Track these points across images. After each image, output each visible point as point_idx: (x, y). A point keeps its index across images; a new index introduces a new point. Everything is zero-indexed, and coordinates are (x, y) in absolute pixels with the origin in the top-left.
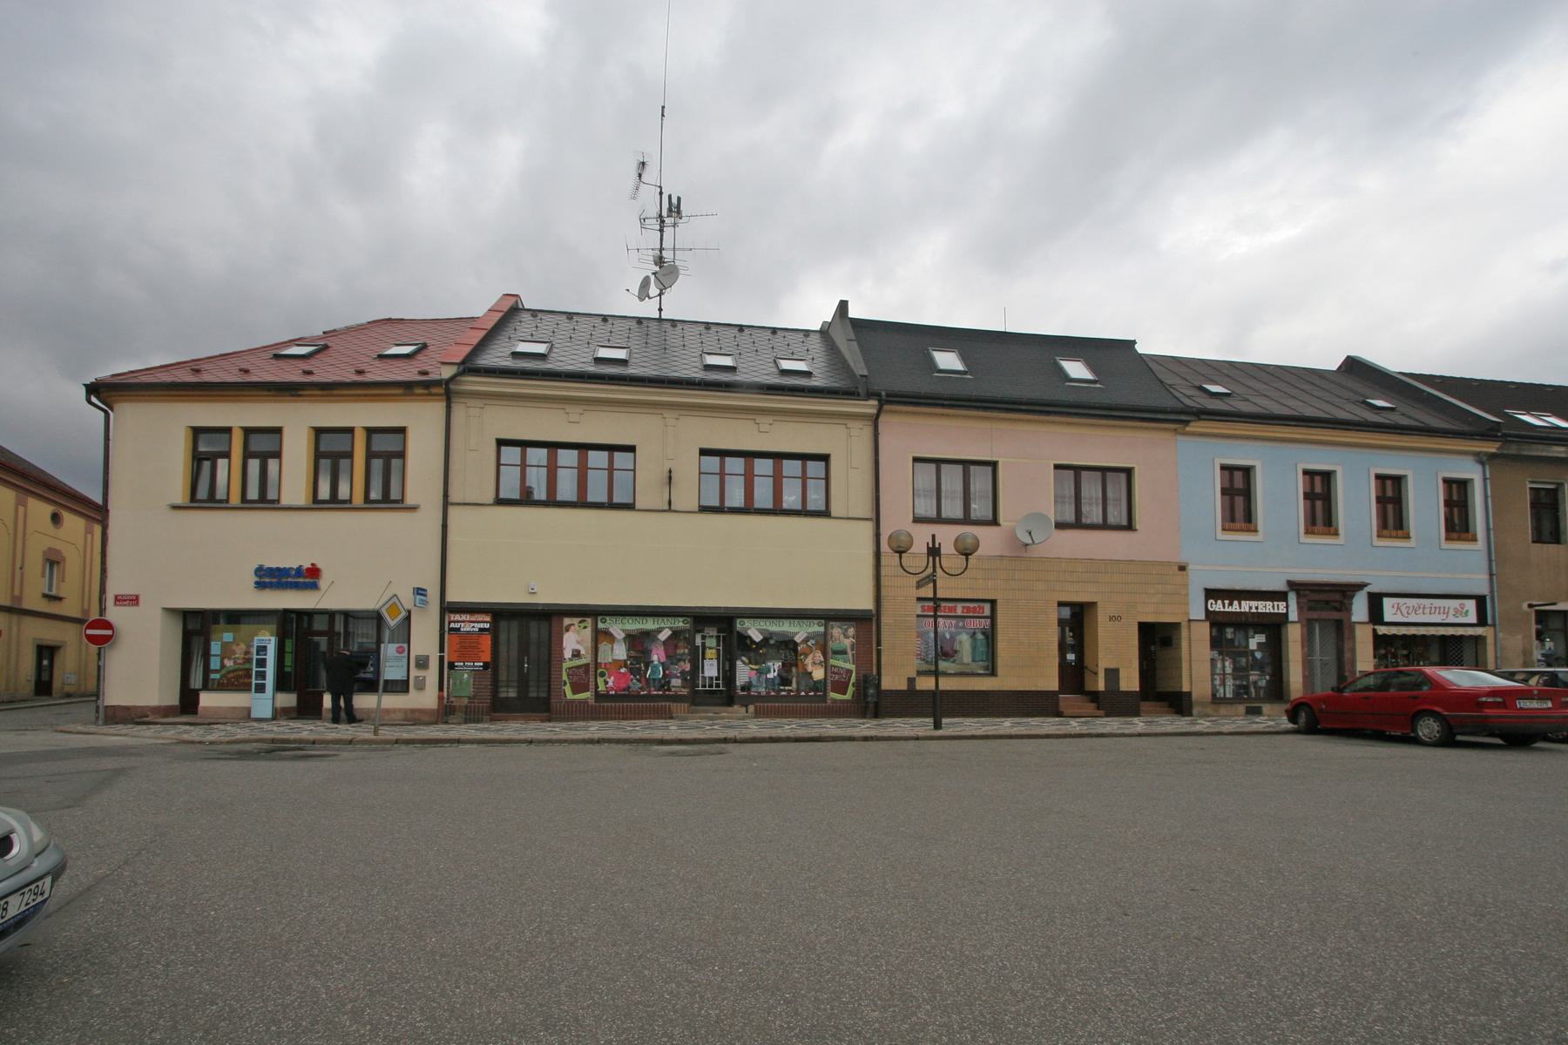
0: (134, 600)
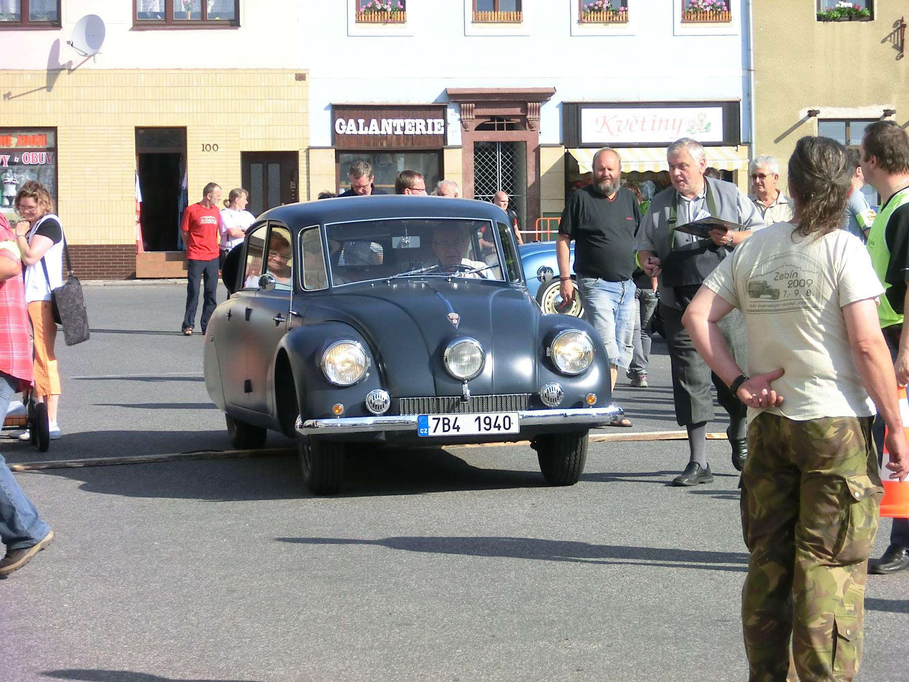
0: (214, 147)
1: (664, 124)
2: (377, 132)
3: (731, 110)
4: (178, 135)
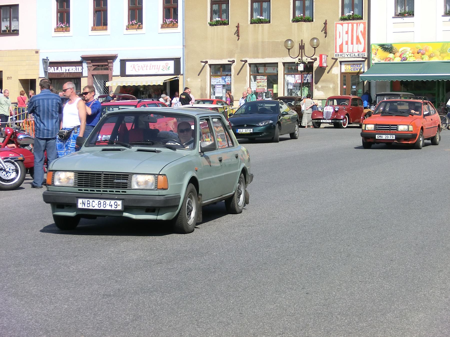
1: (154, 67)
2: (61, 72)
3: (177, 61)
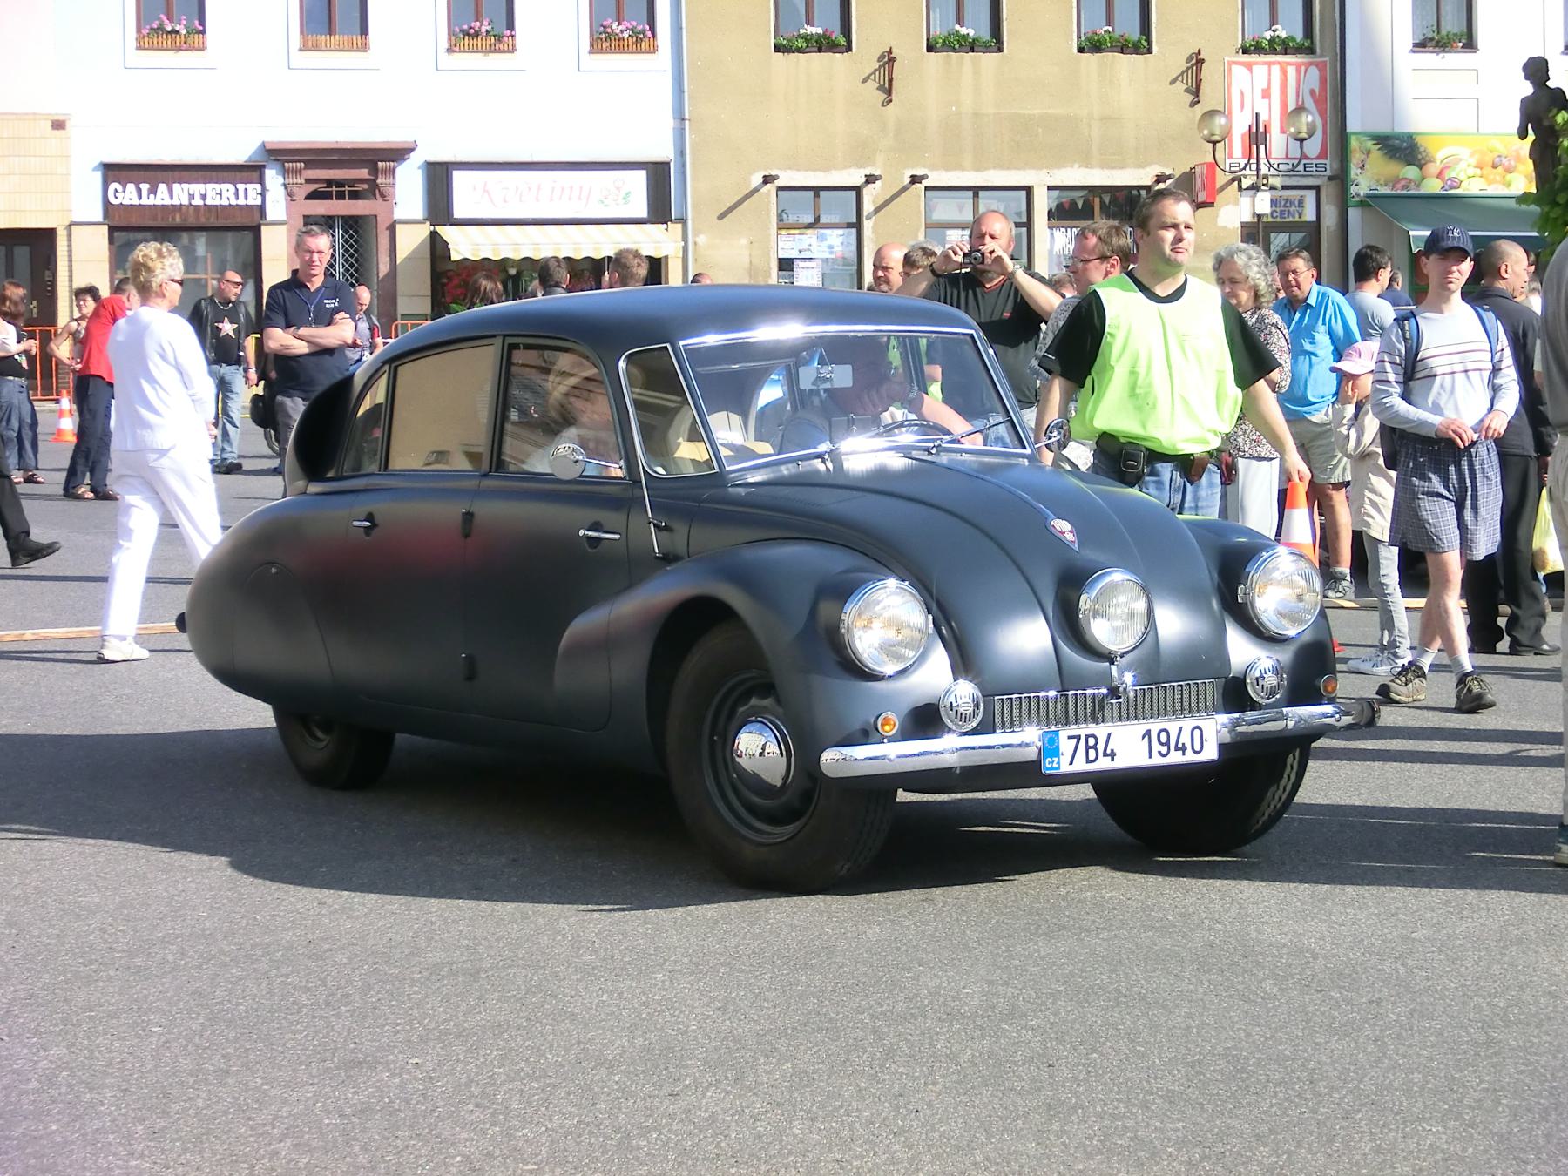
4: (603, 41)
